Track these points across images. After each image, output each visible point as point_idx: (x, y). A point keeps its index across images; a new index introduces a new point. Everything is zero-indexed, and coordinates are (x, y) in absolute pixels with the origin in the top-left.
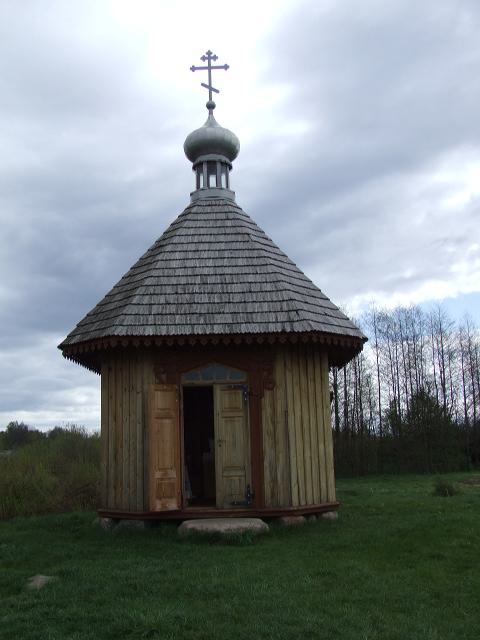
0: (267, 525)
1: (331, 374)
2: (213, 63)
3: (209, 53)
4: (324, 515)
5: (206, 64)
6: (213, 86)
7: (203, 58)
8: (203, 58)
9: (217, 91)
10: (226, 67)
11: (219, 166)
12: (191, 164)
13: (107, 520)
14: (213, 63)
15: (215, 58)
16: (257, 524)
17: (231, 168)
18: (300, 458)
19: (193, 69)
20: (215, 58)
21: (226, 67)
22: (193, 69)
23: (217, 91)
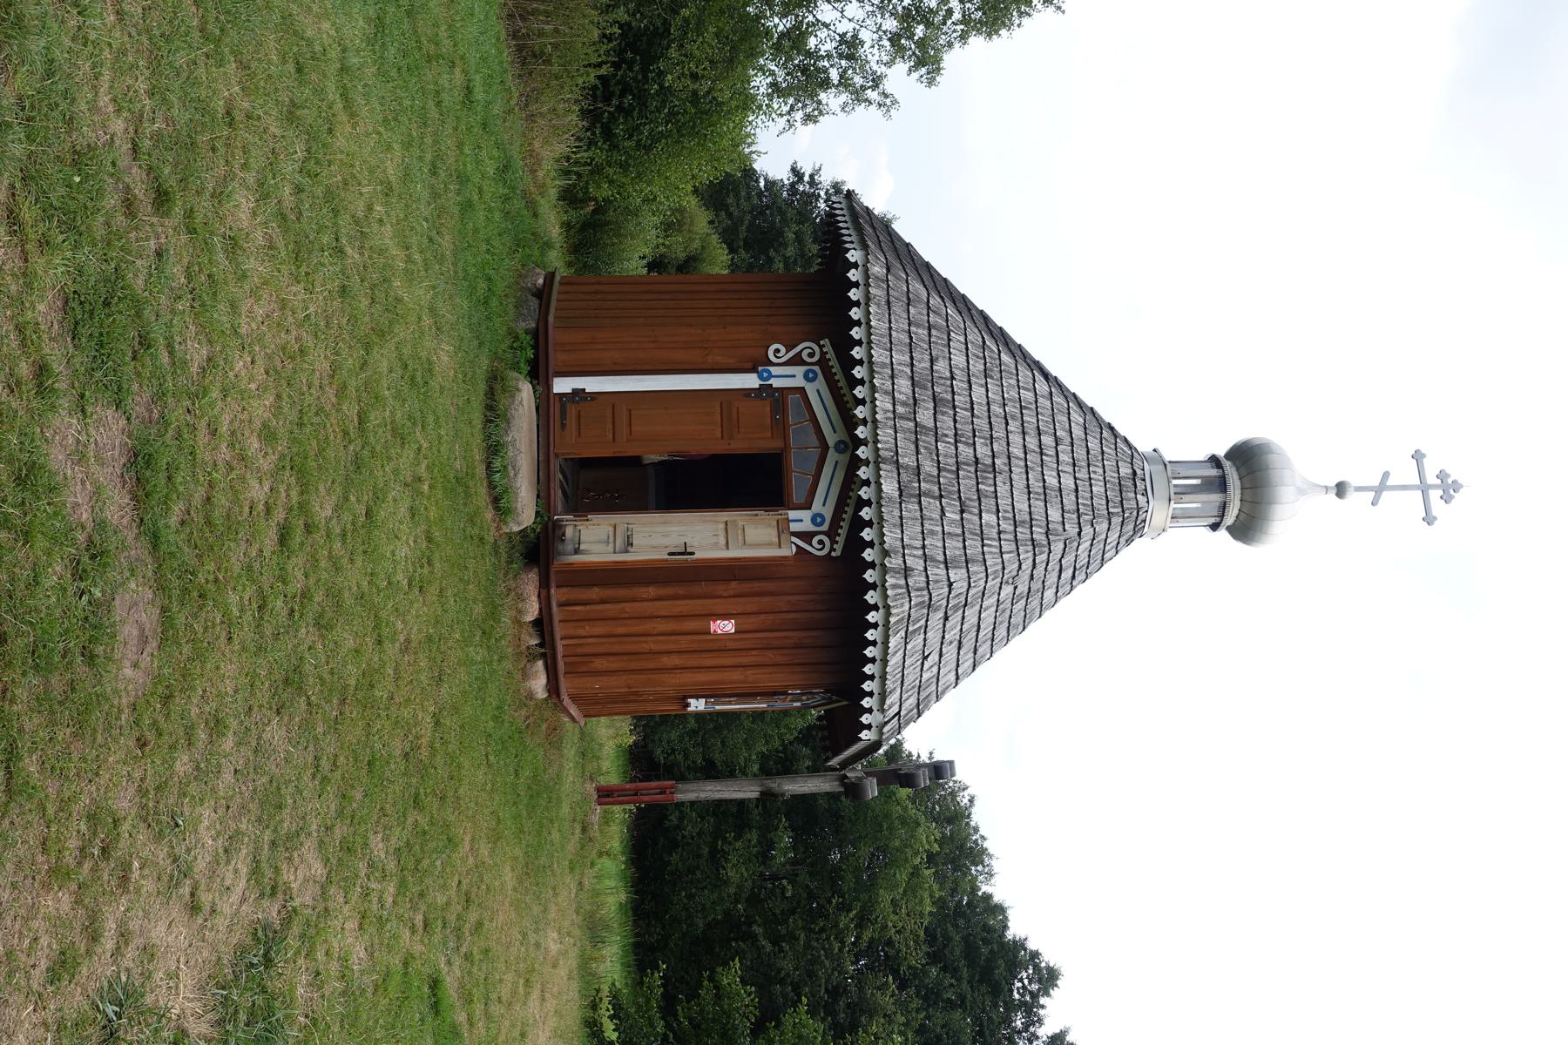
0: (516, 529)
1: (839, 548)
2: (1435, 495)
3: (1456, 486)
4: (540, 663)
5: (1432, 479)
6: (1385, 494)
7: (1442, 476)
8: (1442, 476)
9: (1386, 475)
10: (1429, 519)
11: (1216, 498)
12: (1221, 452)
13: (541, 281)
14: (1435, 495)
15: (1447, 498)
16: (525, 513)
17: (1215, 527)
18: (649, 608)
19: (1418, 456)
20: (1447, 498)
21: (1429, 519)
22: (1418, 456)
23: (1386, 475)
